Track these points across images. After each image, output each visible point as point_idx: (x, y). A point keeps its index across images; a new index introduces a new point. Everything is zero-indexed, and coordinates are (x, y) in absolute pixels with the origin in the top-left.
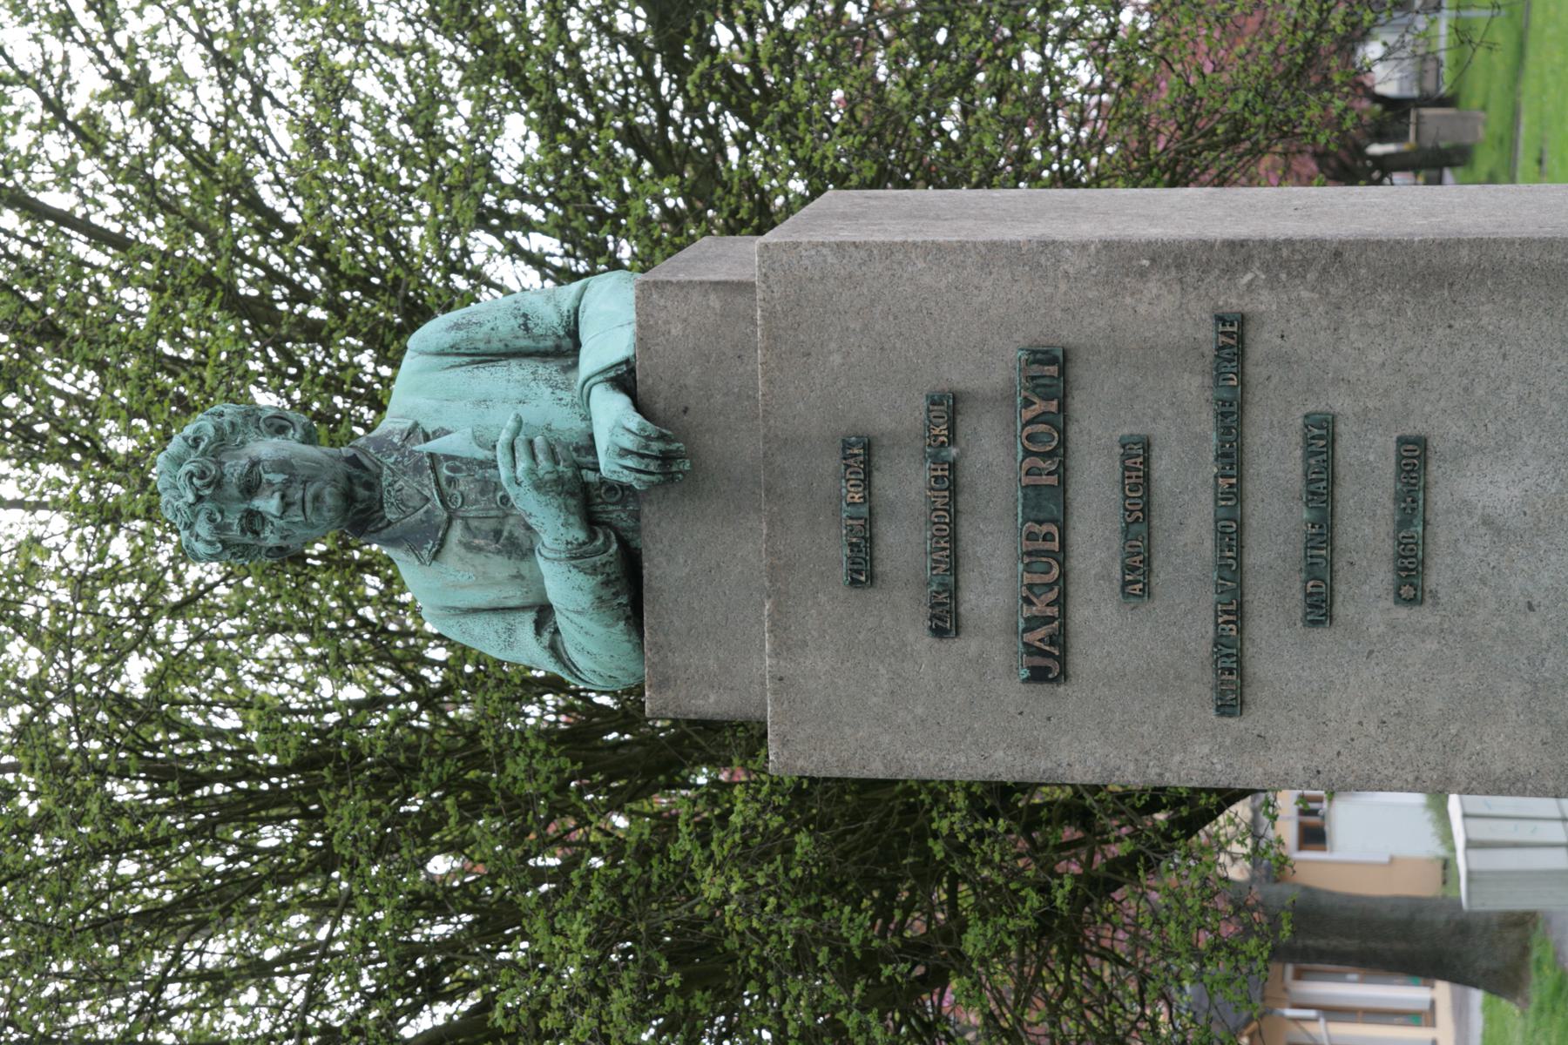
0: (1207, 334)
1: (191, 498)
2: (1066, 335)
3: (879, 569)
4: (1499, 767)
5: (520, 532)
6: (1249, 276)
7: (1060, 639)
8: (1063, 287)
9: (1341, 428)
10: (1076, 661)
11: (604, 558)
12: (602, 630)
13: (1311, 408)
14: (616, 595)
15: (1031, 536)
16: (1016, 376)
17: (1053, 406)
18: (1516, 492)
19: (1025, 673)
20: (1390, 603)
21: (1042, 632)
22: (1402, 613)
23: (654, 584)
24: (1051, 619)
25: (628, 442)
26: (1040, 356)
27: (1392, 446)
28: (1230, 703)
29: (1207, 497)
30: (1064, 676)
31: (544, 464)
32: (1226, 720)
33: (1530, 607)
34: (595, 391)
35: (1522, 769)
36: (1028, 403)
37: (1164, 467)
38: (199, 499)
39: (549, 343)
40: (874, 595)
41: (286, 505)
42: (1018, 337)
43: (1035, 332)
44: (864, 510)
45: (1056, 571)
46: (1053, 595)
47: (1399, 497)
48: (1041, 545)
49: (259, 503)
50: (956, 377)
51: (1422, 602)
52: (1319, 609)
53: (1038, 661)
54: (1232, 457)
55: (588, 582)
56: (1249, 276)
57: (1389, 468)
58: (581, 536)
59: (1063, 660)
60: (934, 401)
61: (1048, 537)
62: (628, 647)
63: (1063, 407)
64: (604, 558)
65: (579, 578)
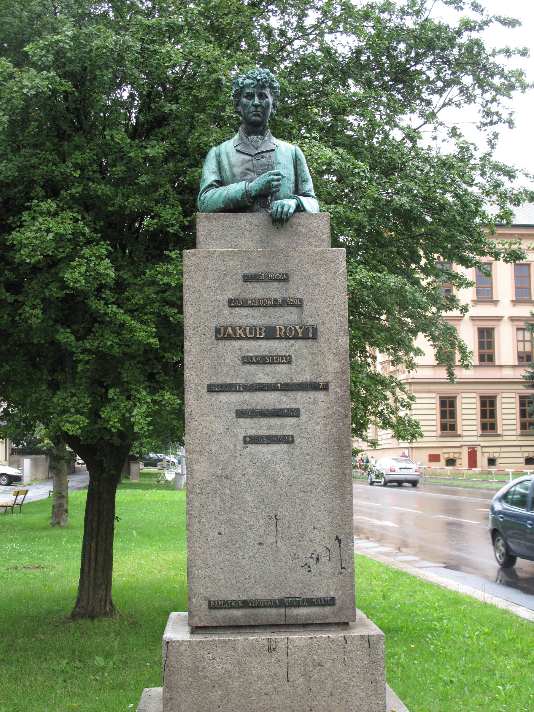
0: (322, 380)
1: (259, 78)
2: (321, 339)
3: (248, 284)
4: (196, 467)
5: (249, 177)
6: (339, 391)
7: (229, 338)
8: (335, 338)
9: (296, 419)
10: (222, 343)
11: (246, 201)
12: (221, 200)
13: (301, 410)
14: (234, 205)
15: (261, 329)
16: (309, 324)
17: (300, 335)
18: (279, 469)
19: (218, 327)
20: (244, 435)
21: (231, 332)
22: (241, 438)
23: (238, 216)
24: (236, 335)
25: (285, 209)
26: (315, 330)
27: (291, 433)
28: (211, 389)
29: (273, 381)
30: (217, 339)
31: (275, 183)
32: (206, 387)
33: (244, 475)
34: (295, 200)
35: (194, 473)
36: (301, 328)
37: (283, 368)
38: (258, 81)
39: (300, 187)
40: (241, 282)
41: (256, 106)
42: (320, 325)
43: (322, 329)
44: (267, 279)
45: (250, 336)
46: (243, 335)
47: (276, 436)
48: (258, 332)
49: (256, 98)
50: (307, 306)
51: (244, 443)
52: (241, 414)
53: (222, 330)
54: (287, 388)
55: (239, 196)
56: (339, 391)
57: (285, 433)
58: (253, 194)
59: (223, 339)
60: (301, 300)
61: (261, 334)
62: (215, 208)
63: (300, 338)
64: (246, 201)
65: (240, 194)
